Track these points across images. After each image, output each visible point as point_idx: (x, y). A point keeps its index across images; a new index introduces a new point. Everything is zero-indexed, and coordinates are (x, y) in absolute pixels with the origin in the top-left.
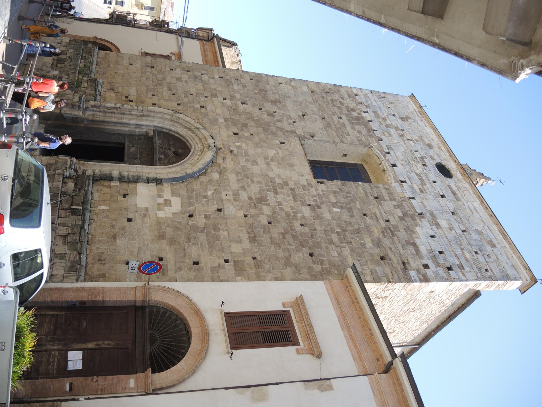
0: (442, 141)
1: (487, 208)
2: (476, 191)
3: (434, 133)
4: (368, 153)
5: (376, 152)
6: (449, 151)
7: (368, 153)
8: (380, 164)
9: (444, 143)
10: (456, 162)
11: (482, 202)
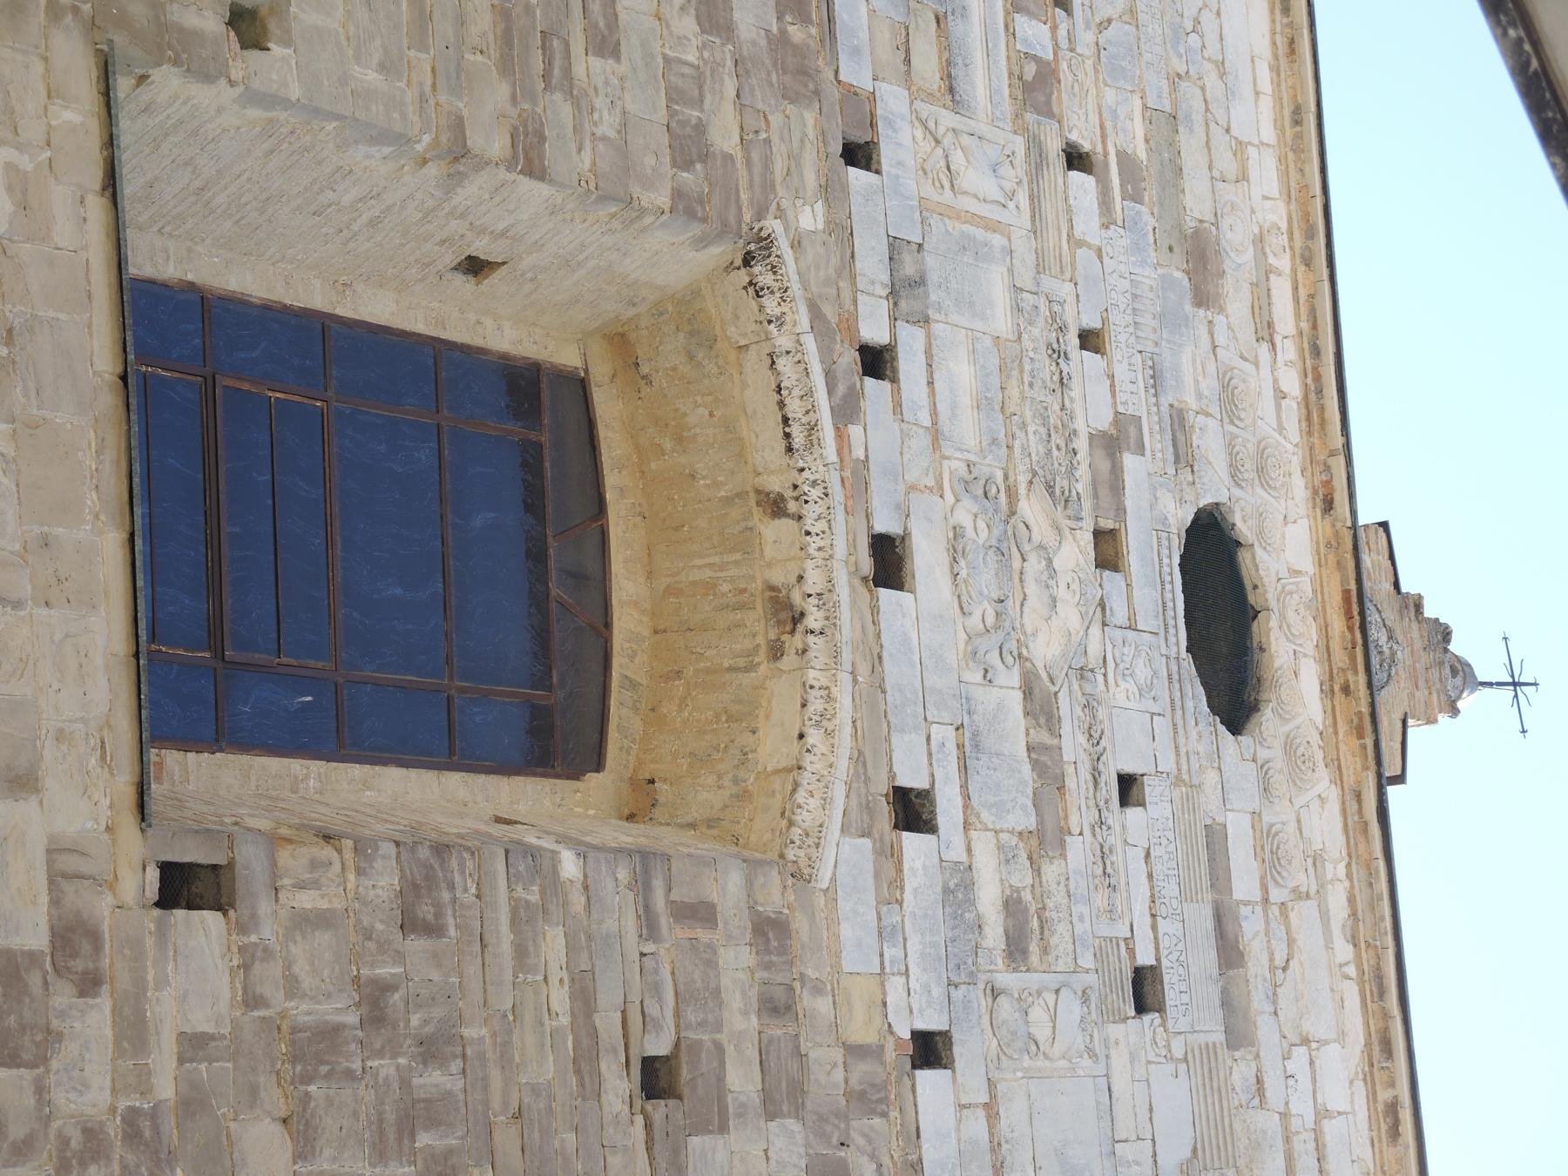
0: (1306, 217)
1: (1394, 1132)
2: (1373, 906)
3: (1275, 69)
4: (697, 293)
5: (783, 341)
6: (1316, 351)
7: (697, 293)
8: (776, 507)
9: (1310, 234)
10: (1328, 505)
11: (1376, 1048)
